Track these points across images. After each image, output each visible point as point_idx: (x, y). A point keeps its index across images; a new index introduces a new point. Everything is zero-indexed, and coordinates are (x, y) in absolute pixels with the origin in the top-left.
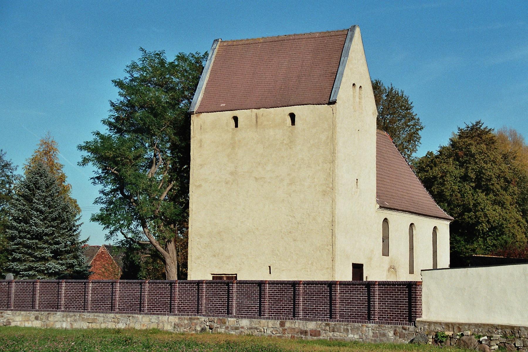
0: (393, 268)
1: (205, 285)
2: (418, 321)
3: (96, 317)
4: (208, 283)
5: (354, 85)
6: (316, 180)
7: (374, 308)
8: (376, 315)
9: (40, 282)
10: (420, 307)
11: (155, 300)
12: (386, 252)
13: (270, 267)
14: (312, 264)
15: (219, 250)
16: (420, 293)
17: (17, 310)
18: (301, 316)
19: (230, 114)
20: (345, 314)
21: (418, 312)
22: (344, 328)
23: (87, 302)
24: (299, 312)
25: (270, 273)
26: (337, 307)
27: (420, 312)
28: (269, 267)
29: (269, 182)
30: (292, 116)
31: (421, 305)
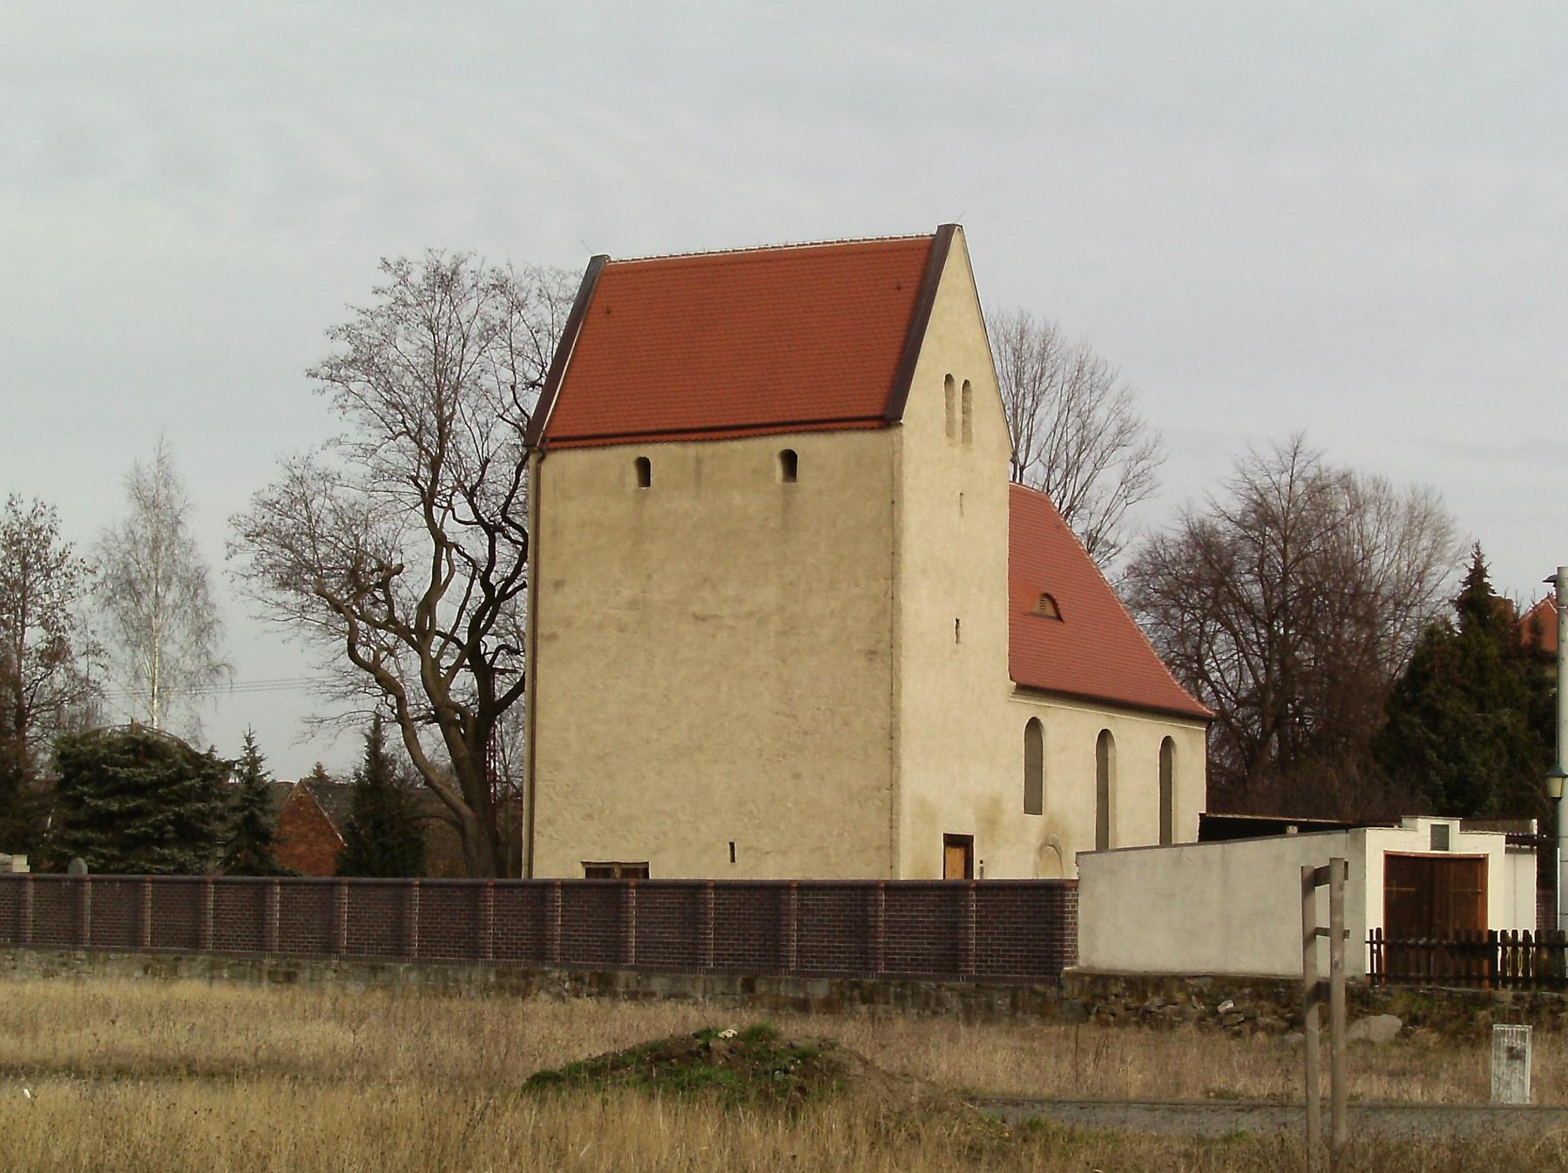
0: (1051, 846)
1: (559, 892)
2: (1067, 973)
3: (292, 970)
4: (568, 887)
5: (949, 378)
6: (849, 622)
7: (967, 944)
8: (972, 961)
9: (153, 881)
10: (1073, 941)
11: (987, 939)
12: (1034, 803)
13: (732, 845)
14: (840, 835)
15: (602, 802)
16: (1073, 907)
17: (100, 950)
18: (793, 966)
19: (632, 453)
20: (900, 959)
21: (1067, 952)
22: (895, 992)
23: (270, 932)
24: (788, 956)
25: (733, 860)
26: (880, 943)
27: (1073, 952)
28: (729, 847)
29: (731, 628)
30: (790, 459)
31: (1076, 935)
